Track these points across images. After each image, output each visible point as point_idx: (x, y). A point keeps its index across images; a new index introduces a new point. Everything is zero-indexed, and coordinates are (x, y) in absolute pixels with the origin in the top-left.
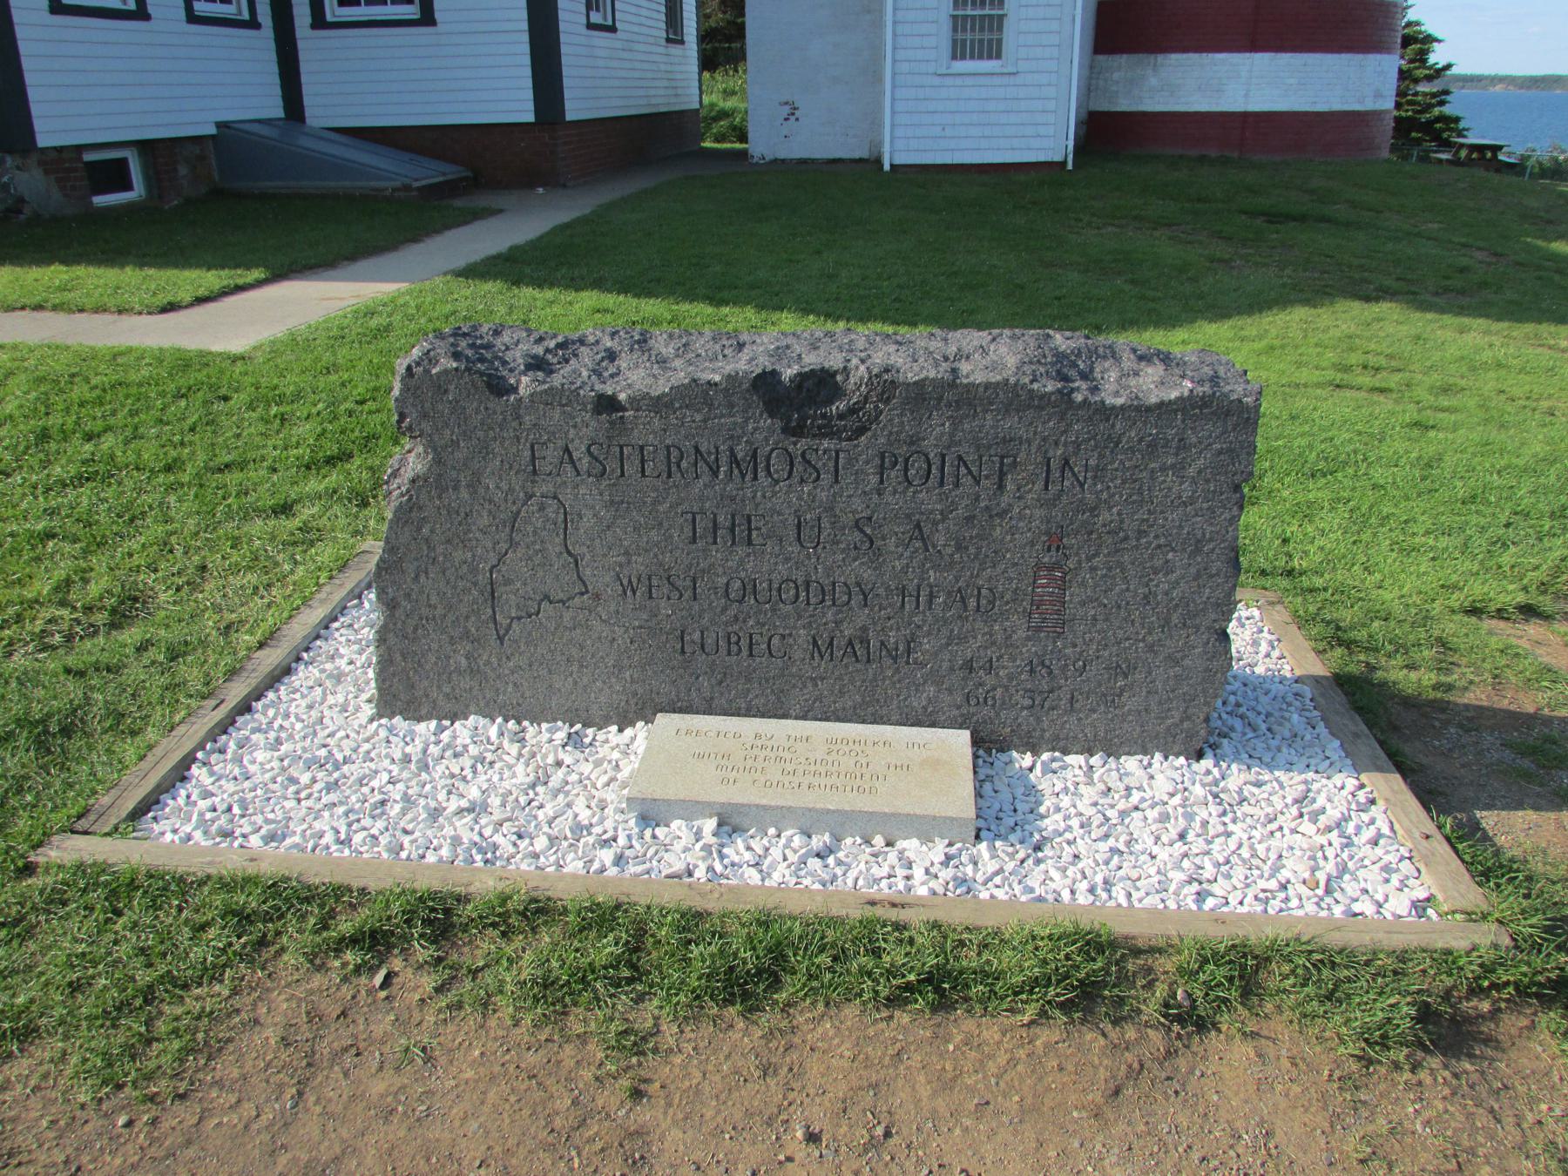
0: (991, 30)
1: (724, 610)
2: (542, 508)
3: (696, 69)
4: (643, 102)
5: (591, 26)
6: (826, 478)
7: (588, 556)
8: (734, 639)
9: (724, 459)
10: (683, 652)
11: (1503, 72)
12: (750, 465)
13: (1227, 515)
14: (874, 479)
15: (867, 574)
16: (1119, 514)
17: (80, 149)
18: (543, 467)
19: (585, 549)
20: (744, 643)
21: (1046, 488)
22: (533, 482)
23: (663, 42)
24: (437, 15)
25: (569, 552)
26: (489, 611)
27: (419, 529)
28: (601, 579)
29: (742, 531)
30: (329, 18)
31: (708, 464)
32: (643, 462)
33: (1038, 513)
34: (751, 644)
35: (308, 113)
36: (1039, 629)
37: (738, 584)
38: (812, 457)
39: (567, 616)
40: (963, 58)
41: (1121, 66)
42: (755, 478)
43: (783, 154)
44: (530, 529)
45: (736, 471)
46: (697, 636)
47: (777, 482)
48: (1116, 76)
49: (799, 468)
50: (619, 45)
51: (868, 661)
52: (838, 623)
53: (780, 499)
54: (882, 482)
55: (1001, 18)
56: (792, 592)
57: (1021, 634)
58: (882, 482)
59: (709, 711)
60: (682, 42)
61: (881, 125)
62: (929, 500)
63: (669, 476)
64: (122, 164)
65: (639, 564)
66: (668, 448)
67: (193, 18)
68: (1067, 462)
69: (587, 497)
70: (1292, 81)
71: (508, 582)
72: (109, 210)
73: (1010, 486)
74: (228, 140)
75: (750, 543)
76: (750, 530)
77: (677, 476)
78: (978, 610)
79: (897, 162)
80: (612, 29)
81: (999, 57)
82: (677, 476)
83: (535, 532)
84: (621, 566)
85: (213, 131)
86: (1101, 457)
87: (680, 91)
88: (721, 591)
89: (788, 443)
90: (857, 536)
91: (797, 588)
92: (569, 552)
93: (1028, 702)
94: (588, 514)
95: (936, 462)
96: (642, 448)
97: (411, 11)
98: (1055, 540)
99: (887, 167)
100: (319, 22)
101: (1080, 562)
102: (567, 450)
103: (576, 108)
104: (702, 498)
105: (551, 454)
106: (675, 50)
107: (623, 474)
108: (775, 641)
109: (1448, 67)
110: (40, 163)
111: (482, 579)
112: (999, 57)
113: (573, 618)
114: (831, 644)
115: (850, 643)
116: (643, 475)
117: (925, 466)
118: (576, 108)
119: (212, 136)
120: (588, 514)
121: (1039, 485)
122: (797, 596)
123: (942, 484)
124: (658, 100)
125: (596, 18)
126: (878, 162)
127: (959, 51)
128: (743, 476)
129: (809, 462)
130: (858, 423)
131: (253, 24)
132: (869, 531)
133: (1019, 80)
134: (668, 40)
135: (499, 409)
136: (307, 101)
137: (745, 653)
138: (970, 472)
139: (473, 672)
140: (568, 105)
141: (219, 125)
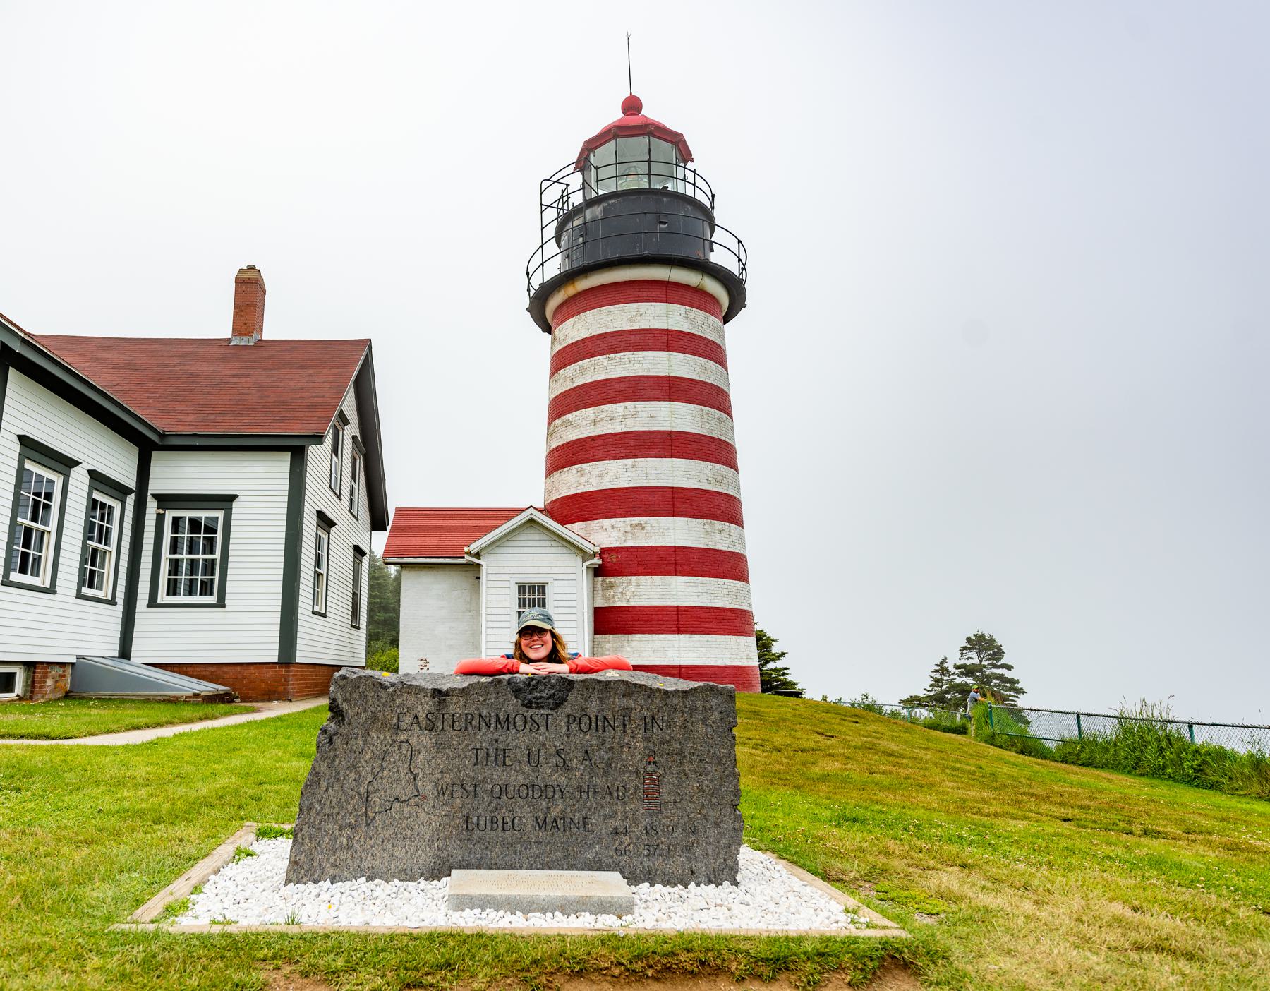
2: (400, 748)
5: (314, 612)
6: (542, 729)
9: (493, 720)
12: (506, 723)
14: (564, 729)
15: (562, 780)
18: (403, 726)
20: (500, 823)
24: (227, 602)
27: (333, 761)
28: (428, 788)
29: (502, 757)
30: (159, 601)
37: (498, 788)
38: (535, 718)
41: (610, 640)
46: (475, 820)
52: (548, 808)
53: (518, 741)
62: (591, 740)
67: (80, 596)
69: (422, 740)
71: (376, 791)
73: (629, 731)
75: (504, 764)
80: (324, 616)
90: (558, 759)
93: (646, 852)
94: (423, 751)
95: (593, 719)
98: (651, 758)
100: (153, 603)
102: (416, 717)
103: (303, 655)
105: (407, 719)
106: (354, 632)
111: (362, 791)
118: (303, 655)
119: (73, 664)
120: (423, 751)
121: (642, 730)
123: (597, 729)
125: (317, 609)
139: (349, 847)
140: (298, 653)
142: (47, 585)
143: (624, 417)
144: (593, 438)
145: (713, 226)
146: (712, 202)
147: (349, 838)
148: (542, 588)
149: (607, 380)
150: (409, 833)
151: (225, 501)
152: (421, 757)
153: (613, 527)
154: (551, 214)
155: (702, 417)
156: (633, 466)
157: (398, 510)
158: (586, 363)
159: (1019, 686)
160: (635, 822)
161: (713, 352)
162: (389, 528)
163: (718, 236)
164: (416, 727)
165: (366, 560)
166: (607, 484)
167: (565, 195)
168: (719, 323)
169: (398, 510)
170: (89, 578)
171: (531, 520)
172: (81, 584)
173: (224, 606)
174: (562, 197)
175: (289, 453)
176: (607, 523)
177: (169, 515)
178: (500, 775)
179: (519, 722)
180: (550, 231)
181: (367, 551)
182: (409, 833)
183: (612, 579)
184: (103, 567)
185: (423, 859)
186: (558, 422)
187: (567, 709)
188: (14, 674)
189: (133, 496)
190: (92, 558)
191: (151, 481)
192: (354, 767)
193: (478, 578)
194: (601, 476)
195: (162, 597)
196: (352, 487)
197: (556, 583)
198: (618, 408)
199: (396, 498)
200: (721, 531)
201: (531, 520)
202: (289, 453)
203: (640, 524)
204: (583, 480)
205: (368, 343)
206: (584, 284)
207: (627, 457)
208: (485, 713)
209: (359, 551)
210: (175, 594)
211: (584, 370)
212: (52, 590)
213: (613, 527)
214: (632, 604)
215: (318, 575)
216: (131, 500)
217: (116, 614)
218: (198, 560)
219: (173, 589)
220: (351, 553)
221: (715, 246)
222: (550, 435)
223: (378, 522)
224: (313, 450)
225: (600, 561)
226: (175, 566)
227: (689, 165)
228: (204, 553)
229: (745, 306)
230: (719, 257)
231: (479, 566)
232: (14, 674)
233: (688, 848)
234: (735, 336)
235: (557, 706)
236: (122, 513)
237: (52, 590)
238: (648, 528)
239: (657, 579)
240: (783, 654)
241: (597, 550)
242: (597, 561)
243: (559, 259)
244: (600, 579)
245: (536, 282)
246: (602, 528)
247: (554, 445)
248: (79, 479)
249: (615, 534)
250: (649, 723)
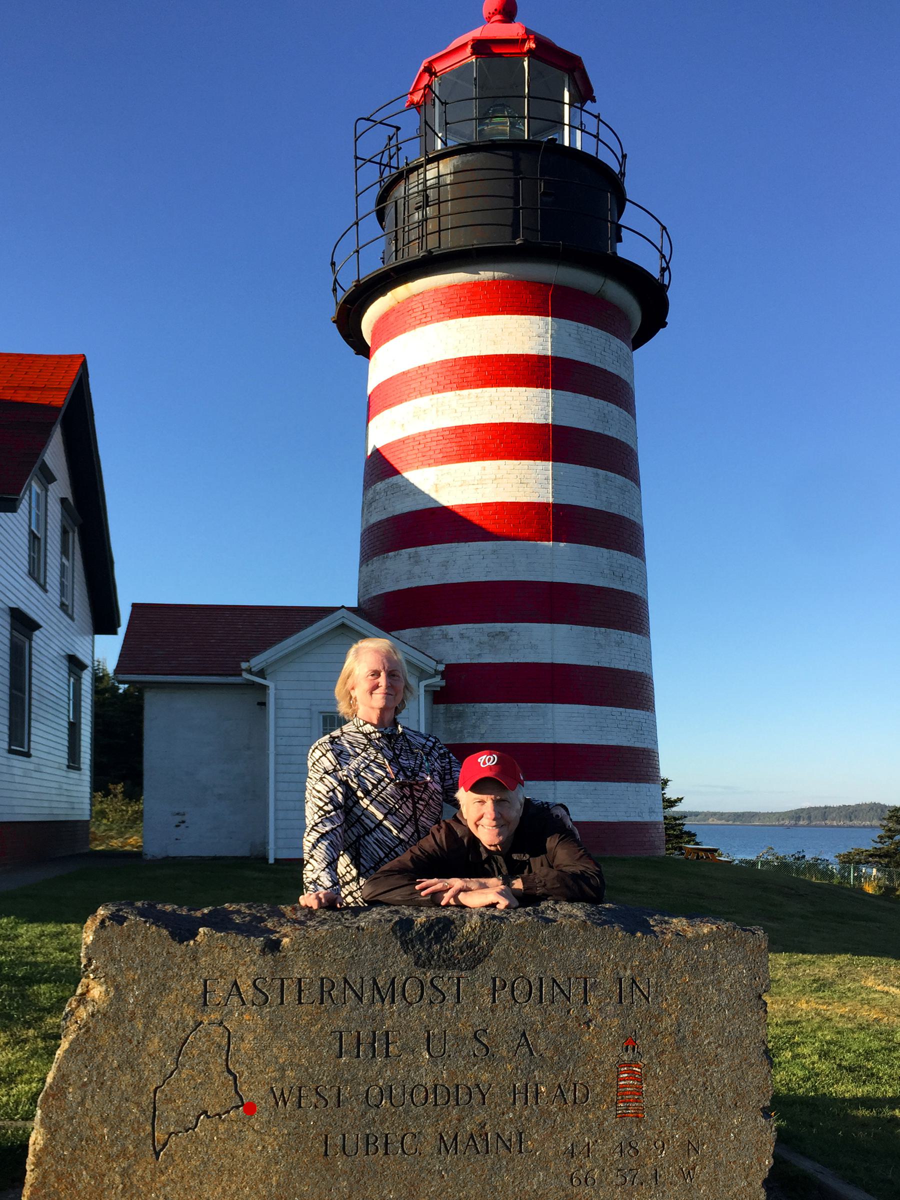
1: (363, 1115)
3: (88, 790)
4: (47, 811)
5: (11, 751)
6: (450, 1000)
7: (246, 1074)
8: (371, 1140)
9: (368, 983)
10: (326, 1154)
11: (712, 810)
12: (390, 992)
13: (756, 1017)
16: (677, 1018)
19: (244, 1068)
21: (621, 1002)
22: (203, 1011)
23: (65, 768)
25: (229, 1071)
26: (149, 1128)
29: (378, 1044)
31: (354, 991)
32: (300, 991)
33: (616, 1022)
34: (386, 1144)
36: (623, 1116)
37: (377, 1090)
39: (222, 1128)
42: (393, 1002)
43: (173, 853)
44: (195, 1052)
45: (377, 996)
46: (339, 1142)
47: (411, 1004)
49: (428, 991)
50: (31, 767)
51: (487, 1152)
54: (494, 1001)
56: (423, 1095)
57: (611, 1120)
58: (494, 1001)
60: (79, 769)
61: (266, 828)
63: (322, 1003)
66: (322, 979)
68: (634, 982)
70: (588, 801)
71: (169, 1100)
73: (592, 1001)
75: (387, 1056)
76: (388, 1044)
77: (328, 1002)
78: (575, 1102)
79: (278, 857)
82: (328, 1002)
83: (200, 1055)
84: (276, 1080)
86: (659, 976)
87: (76, 806)
88: (362, 1098)
89: (418, 973)
91: (426, 1091)
92: (229, 1071)
93: (620, 1180)
96: (300, 980)
99: (271, 861)
101: (651, 1058)
104: (347, 1020)
106: (73, 774)
107: (282, 1003)
108: (408, 1139)
109: (680, 800)
111: (145, 1100)
113: (227, 1130)
114: (455, 1138)
115: (472, 1137)
116: (300, 1003)
117: (527, 987)
122: (426, 1098)
124: (61, 811)
126: (265, 859)
128: (383, 1000)
129: (436, 987)
130: (475, 955)
132: (485, 1042)
134: (69, 767)
135: (179, 953)
137: (381, 1151)
138: (562, 991)
145: (621, 200)
146: (622, 165)
147: (124, 1173)
150: (226, 1161)
152: (245, 1046)
153: (462, 636)
154: (371, 174)
155: (597, 484)
157: (134, 606)
160: (605, 1135)
161: (614, 390)
162: (122, 630)
163: (630, 217)
164: (235, 1000)
165: (87, 678)
166: (455, 576)
167: (393, 146)
168: (626, 348)
169: (134, 606)
171: (343, 625)
174: (388, 147)
176: (453, 630)
179: (412, 990)
180: (369, 202)
181: (88, 662)
182: (226, 1161)
183: (460, 707)
186: (380, 486)
187: (490, 968)
192: (129, 1064)
193: (263, 704)
194: (445, 564)
196: (63, 565)
199: (132, 588)
201: (343, 625)
203: (502, 633)
204: (417, 570)
205: (83, 363)
208: (353, 977)
209: (75, 664)
213: (462, 636)
220: (64, 666)
221: (624, 233)
222: (367, 505)
223: (104, 622)
225: (443, 683)
227: (589, 106)
229: (664, 325)
230: (629, 249)
231: (264, 688)
234: (649, 368)
238: (514, 637)
240: (680, 800)
241: (441, 668)
242: (437, 681)
243: (381, 244)
244: (442, 706)
245: (348, 283)
247: (375, 519)
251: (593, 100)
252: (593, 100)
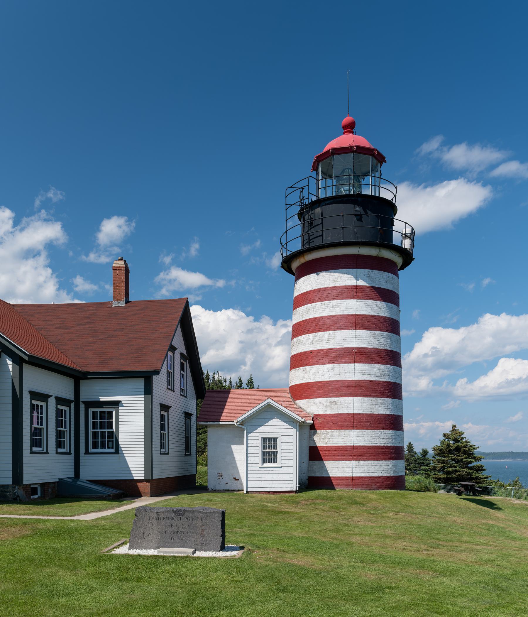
0: (274, 455)
17: (30, 485)
28: (156, 532)
29: (171, 526)
30: (90, 452)
35: (80, 476)
40: (267, 463)
48: (315, 467)
53: (175, 522)
55: (277, 452)
59: (166, 547)
62: (190, 522)
64: (36, 489)
65: (160, 530)
67: (57, 453)
72: (34, 499)
74: (61, 482)
80: (168, 454)
81: (276, 462)
85: (57, 480)
97: (113, 450)
98: (203, 526)
100: (87, 452)
106: (188, 457)
110: (23, 488)
112: (276, 462)
125: (163, 451)
127: (264, 461)
131: (70, 453)
133: (283, 468)
136: (81, 473)
141: (59, 479)
142: (45, 451)
143: (328, 340)
144: (311, 352)
148: (275, 440)
149: (320, 317)
151: (117, 404)
153: (320, 403)
156: (332, 368)
158: (309, 306)
159: (484, 468)
166: (318, 379)
170: (59, 444)
172: (57, 448)
173: (118, 453)
175: (144, 379)
176: (317, 400)
177: (91, 411)
178: (171, 529)
184: (64, 438)
185: (155, 545)
188: (37, 488)
189: (73, 403)
190: (59, 435)
191: (81, 395)
194: (315, 374)
195: (91, 450)
197: (283, 437)
198: (325, 335)
200: (382, 404)
202: (144, 379)
204: (306, 375)
206: (310, 257)
207: (329, 363)
210: (95, 448)
211: (308, 311)
212: (47, 453)
213: (320, 403)
214: (329, 445)
215: (162, 436)
216: (73, 405)
217: (72, 457)
218: (105, 432)
219: (95, 446)
224: (155, 377)
226: (95, 435)
228: (107, 429)
232: (37, 488)
233: (210, 544)
235: (182, 515)
236: (69, 411)
237: (47, 453)
239: (343, 431)
246: (314, 403)
248: (52, 402)
249: (321, 407)
250: (202, 519)
251: (385, 162)
252: (385, 162)
